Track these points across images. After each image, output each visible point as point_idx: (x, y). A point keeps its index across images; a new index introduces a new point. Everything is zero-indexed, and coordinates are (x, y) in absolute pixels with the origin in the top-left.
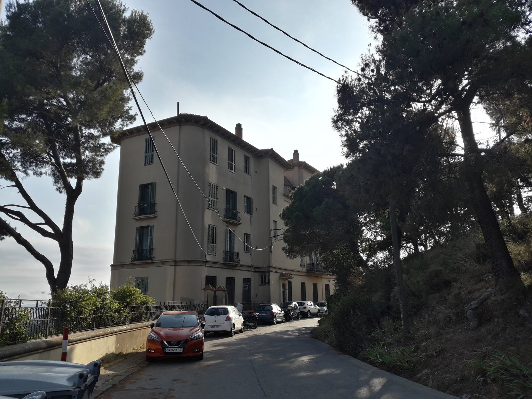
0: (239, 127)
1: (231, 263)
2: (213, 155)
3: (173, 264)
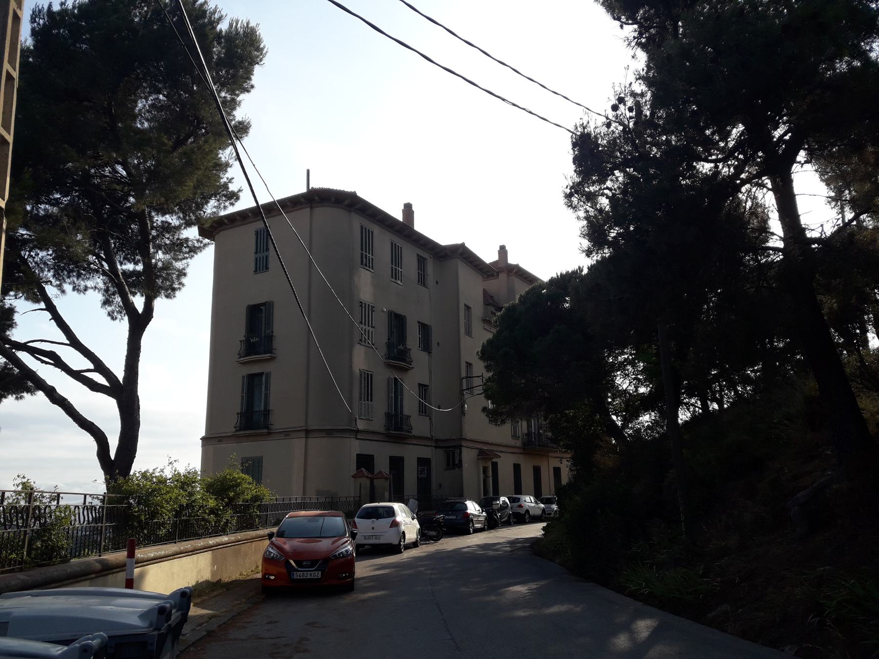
0: (408, 210)
1: (398, 432)
2: (366, 255)
3: (303, 434)
